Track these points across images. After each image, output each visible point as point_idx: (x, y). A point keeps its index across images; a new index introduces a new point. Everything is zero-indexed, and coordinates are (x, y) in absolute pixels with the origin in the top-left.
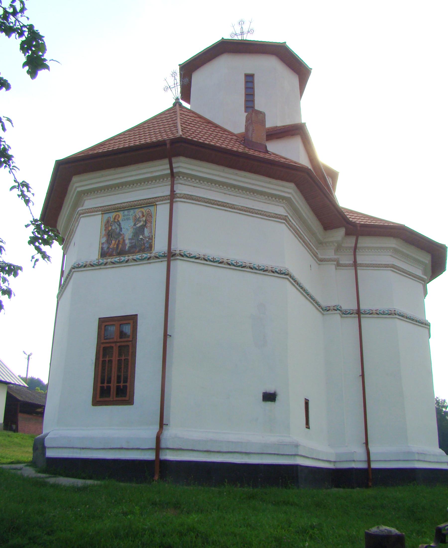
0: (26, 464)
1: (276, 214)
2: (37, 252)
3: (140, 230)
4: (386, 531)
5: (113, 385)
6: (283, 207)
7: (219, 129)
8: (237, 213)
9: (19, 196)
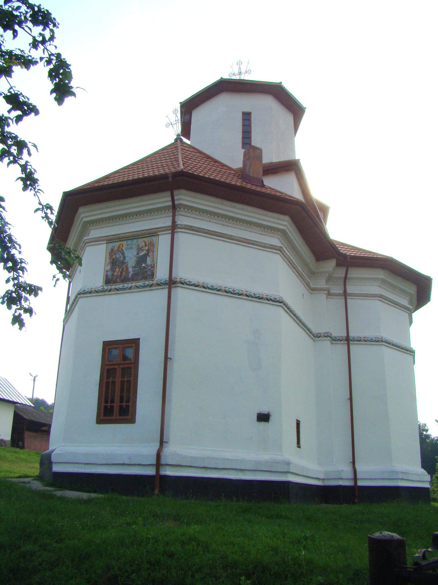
0: (33, 478)
1: (272, 245)
2: (58, 271)
3: (142, 260)
4: (388, 536)
5: (116, 405)
6: (279, 239)
7: (218, 164)
8: (234, 243)
9: (43, 218)
